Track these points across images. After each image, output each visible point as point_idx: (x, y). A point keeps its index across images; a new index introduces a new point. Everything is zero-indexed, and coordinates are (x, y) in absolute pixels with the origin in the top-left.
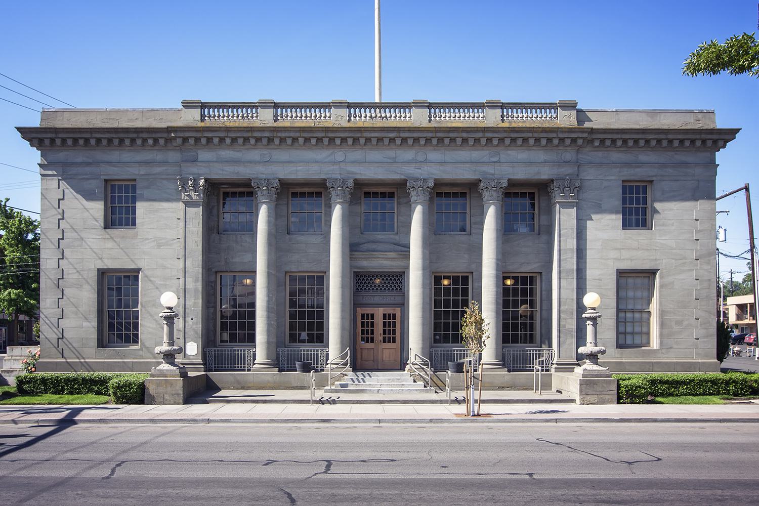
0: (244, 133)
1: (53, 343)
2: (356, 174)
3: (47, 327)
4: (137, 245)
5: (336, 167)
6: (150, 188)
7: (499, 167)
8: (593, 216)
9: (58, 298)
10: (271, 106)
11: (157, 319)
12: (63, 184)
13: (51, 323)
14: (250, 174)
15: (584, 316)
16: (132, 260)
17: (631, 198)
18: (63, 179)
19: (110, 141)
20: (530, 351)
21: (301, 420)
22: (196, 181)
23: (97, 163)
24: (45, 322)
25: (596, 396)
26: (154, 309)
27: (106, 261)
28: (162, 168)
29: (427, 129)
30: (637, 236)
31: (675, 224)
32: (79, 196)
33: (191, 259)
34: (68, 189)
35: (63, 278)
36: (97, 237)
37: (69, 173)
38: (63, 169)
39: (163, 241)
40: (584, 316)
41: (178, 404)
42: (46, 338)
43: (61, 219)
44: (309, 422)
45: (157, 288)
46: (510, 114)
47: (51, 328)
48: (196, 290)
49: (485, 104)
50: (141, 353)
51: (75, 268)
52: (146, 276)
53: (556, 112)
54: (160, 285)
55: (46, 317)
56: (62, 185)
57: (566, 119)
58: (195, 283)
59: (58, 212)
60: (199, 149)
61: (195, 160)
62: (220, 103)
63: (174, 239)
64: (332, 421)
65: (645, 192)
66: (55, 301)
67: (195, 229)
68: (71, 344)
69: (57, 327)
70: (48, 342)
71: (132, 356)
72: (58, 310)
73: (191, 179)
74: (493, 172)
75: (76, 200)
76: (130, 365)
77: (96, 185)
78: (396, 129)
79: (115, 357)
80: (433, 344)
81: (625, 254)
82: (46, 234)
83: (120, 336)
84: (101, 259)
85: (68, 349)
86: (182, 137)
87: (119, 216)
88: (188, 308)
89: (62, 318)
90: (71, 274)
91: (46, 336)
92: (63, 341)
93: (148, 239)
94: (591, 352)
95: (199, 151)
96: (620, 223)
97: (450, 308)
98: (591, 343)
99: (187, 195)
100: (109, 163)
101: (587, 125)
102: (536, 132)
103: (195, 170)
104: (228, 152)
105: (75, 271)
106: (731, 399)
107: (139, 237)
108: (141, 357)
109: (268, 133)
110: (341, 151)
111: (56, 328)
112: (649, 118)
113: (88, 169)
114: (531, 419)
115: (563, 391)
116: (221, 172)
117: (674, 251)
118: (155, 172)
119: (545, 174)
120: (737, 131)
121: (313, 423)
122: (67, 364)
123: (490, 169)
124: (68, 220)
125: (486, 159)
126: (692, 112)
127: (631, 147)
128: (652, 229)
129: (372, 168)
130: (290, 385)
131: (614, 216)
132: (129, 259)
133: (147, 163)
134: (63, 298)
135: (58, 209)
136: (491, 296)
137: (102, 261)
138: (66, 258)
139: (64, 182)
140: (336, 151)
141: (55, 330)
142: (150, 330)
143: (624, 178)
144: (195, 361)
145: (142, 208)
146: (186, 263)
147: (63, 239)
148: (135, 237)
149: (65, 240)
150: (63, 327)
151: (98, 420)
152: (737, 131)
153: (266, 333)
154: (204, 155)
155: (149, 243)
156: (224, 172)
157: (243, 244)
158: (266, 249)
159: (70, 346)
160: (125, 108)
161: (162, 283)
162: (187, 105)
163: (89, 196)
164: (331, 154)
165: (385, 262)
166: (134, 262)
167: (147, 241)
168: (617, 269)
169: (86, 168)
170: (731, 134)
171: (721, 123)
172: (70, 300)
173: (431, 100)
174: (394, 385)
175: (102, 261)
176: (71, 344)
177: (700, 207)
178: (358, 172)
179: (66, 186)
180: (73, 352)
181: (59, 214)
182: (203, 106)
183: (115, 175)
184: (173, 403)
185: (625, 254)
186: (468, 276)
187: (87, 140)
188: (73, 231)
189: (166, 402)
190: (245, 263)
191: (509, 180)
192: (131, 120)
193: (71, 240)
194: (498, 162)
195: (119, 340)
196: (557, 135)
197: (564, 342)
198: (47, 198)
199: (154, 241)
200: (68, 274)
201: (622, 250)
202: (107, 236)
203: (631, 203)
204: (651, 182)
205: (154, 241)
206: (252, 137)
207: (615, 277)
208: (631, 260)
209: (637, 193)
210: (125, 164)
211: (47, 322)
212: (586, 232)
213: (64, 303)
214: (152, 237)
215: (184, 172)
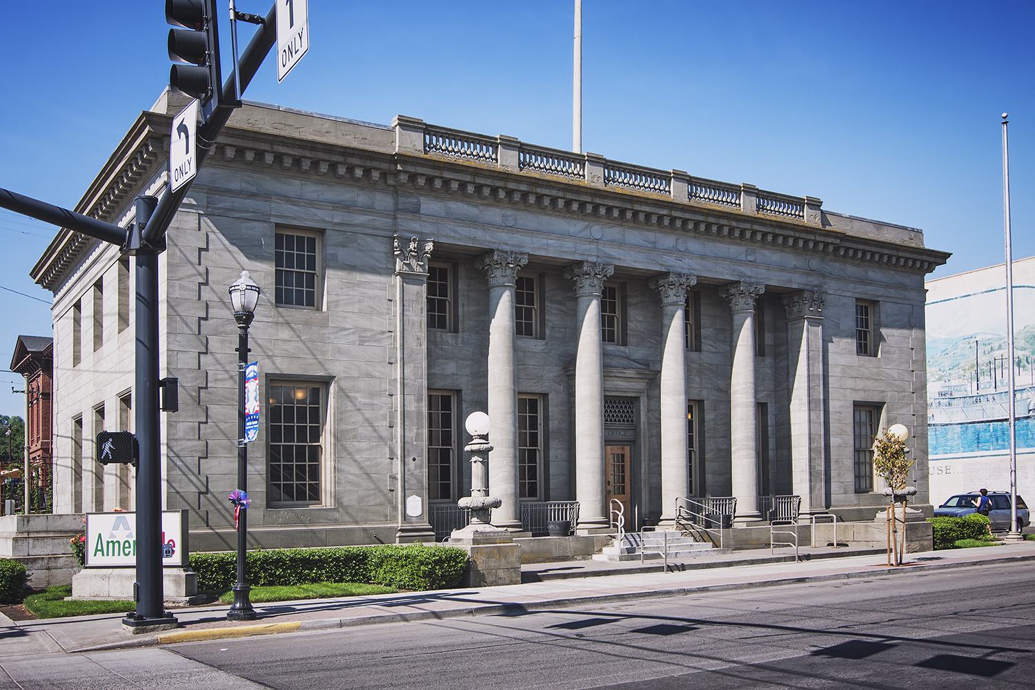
0: (496, 181)
3: (180, 473)
4: (329, 338)
6: (347, 247)
7: (755, 269)
10: (516, 147)
11: (359, 460)
12: (206, 223)
13: (186, 466)
14: (489, 242)
15: (467, 448)
16: (320, 363)
18: (206, 215)
20: (566, 506)
21: (778, 581)
23: (267, 196)
24: (176, 464)
25: (918, 542)
27: (278, 361)
28: (368, 217)
29: (701, 210)
30: (865, 359)
31: (896, 352)
32: (234, 249)
33: (413, 364)
34: (213, 232)
36: (265, 319)
38: (208, 198)
39: (368, 334)
40: (467, 448)
43: (203, 284)
44: (786, 584)
46: (434, 143)
47: (185, 475)
48: (419, 413)
49: (672, 175)
50: (337, 515)
52: (341, 389)
55: (178, 456)
56: (204, 224)
57: (809, 218)
58: (418, 403)
59: (198, 272)
60: (423, 195)
61: (416, 211)
62: (450, 130)
63: (384, 332)
64: (807, 580)
65: (312, 248)
68: (221, 504)
69: (197, 472)
70: (181, 500)
71: (321, 521)
72: (196, 443)
73: (414, 240)
74: (750, 274)
77: (263, 232)
78: (670, 205)
82: (177, 308)
83: (288, 490)
85: (216, 511)
86: (490, 186)
87: (296, 288)
88: (408, 442)
89: (206, 458)
91: (177, 489)
94: (483, 503)
95: (421, 198)
97: (281, 442)
98: (479, 491)
101: (828, 228)
103: (416, 226)
104: (461, 205)
105: (227, 376)
108: (336, 521)
109: (526, 186)
110: (598, 224)
111: (194, 475)
112: (875, 230)
113: (250, 203)
114: (962, 563)
115: (848, 543)
116: (453, 235)
117: (896, 382)
118: (355, 222)
119: (796, 282)
121: (790, 583)
122: (217, 537)
123: (747, 271)
124: (214, 287)
125: (743, 257)
126: (905, 228)
129: (632, 253)
130: (550, 555)
131: (850, 340)
132: (315, 360)
133: (347, 207)
134: (206, 423)
135: (197, 266)
136: (750, 430)
138: (211, 353)
140: (592, 224)
141: (193, 478)
145: (333, 282)
146: (405, 371)
147: (206, 319)
148: (324, 324)
149: (210, 322)
150: (207, 472)
151: (554, 601)
152: (949, 255)
154: (429, 205)
155: (346, 335)
156: (457, 235)
157: (443, 347)
159: (220, 507)
160: (839, 213)
161: (367, 401)
162: (407, 124)
164: (586, 227)
165: (620, 383)
166: (323, 366)
167: (344, 333)
168: (854, 401)
170: (942, 257)
171: (929, 243)
172: (217, 426)
173: (609, 156)
174: (683, 546)
176: (221, 504)
177: (915, 333)
178: (618, 256)
179: (210, 227)
180: (224, 516)
181: (200, 274)
182: (428, 130)
183: (294, 219)
184: (509, 582)
185: (860, 384)
186: (537, 400)
187: (260, 154)
188: (223, 306)
190: (448, 375)
193: (220, 321)
196: (752, 227)
197: (815, 487)
198: (179, 244)
199: (353, 333)
200: (216, 380)
201: (857, 379)
202: (281, 320)
203: (290, 265)
204: (322, 232)
206: (502, 188)
208: (865, 391)
209: (301, 248)
210: (309, 202)
211: (179, 463)
212: (828, 355)
213: (208, 431)
214: (352, 327)
215: (402, 228)
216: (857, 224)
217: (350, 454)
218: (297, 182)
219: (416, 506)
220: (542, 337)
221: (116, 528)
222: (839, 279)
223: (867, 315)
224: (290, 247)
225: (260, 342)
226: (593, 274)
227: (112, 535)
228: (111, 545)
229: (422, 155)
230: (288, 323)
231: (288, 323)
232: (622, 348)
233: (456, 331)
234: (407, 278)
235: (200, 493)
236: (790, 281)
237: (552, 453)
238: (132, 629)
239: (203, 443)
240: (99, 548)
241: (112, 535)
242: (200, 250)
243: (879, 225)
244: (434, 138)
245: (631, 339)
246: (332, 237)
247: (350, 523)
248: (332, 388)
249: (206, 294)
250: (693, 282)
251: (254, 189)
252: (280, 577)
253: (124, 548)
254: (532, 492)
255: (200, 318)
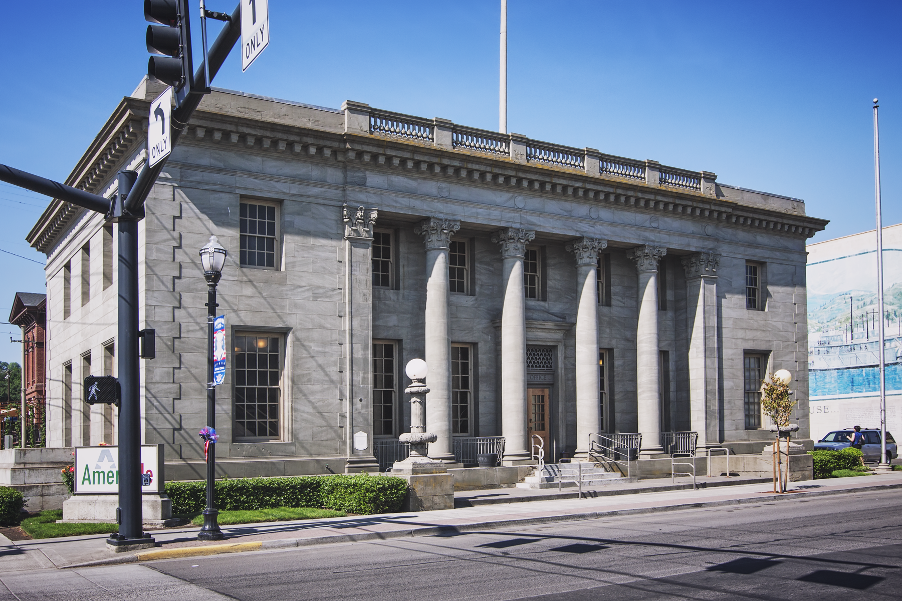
1: (166, 437)
2: (536, 225)
5: (517, 215)
8: (727, 296)
9: (174, 368)
10: (449, 128)
14: (427, 211)
16: (279, 316)
17: (253, 223)
18: (180, 187)
19: (259, 140)
22: (367, 212)
23: (233, 171)
26: (310, 387)
27: (242, 314)
32: (204, 217)
35: (180, 338)
37: (191, 179)
39: (321, 291)
40: (407, 390)
41: (450, 508)
42: (155, 429)
45: (313, 357)
48: (365, 360)
50: (293, 449)
51: (197, 323)
53: (432, 132)
54: (318, 352)
55: (155, 397)
57: (705, 190)
60: (369, 170)
66: (168, 373)
67: (363, 278)
68: (193, 439)
69: (171, 411)
72: (171, 385)
75: (198, 221)
76: (282, 467)
77: (229, 203)
79: (257, 456)
80: (393, 436)
81: (750, 335)
84: (234, 311)
89: (180, 399)
90: (193, 331)
92: (181, 435)
93: (301, 287)
96: (744, 302)
99: (354, 230)
100: (250, 173)
101: (721, 198)
102: (695, 201)
103: (362, 197)
105: (197, 328)
106: (369, 522)
107: (288, 283)
108: (293, 454)
113: (218, 177)
118: (309, 193)
119: (694, 245)
120: (826, 222)
122: (189, 468)
123: (651, 236)
124: (187, 250)
126: (789, 199)
127: (251, 147)
128: (763, 310)
131: (740, 297)
133: (303, 180)
134: (180, 368)
137: (238, 315)
138: (184, 308)
139: (181, 192)
141: (168, 416)
142: (305, 415)
143: (747, 258)
144: (365, 458)
147: (180, 278)
149: (183, 280)
150: (180, 412)
152: (826, 222)
153: (447, 419)
154: (374, 179)
158: (446, 310)
159: (191, 441)
161: (320, 349)
162: (355, 108)
163: (220, 219)
165: (540, 334)
167: (300, 290)
169: (215, 175)
170: (820, 224)
173: (456, 121)
175: (238, 315)
176: (193, 439)
177: (797, 290)
178: (538, 223)
181: (174, 239)
182: (373, 113)
183: (256, 190)
185: (750, 335)
187: (226, 135)
189: (436, 507)
191: (668, 249)
192: (277, 115)
194: (657, 228)
195: (250, 433)
199: (308, 290)
200: (188, 331)
202: (245, 278)
204: (280, 202)
205: (308, 290)
207: (742, 357)
208: (754, 340)
209: (262, 216)
210: (270, 176)
211: (156, 403)
213: (182, 375)
216: (747, 196)
217: (305, 395)
218: (259, 159)
219: (362, 441)
220: (473, 294)
221: (101, 459)
222: (731, 242)
223: (755, 274)
224: (253, 215)
225: (227, 298)
226: (516, 238)
227: (98, 466)
228: (96, 474)
229: (368, 135)
230: (251, 281)
231: (251, 281)
232: (542, 303)
233: (397, 288)
234: (355, 242)
235: (174, 429)
236: (688, 245)
237: (481, 395)
238: (115, 548)
239: (176, 386)
240: (87, 477)
241: (98, 466)
242: (175, 218)
243: (766, 196)
244: (378, 120)
245: (550, 296)
246: (289, 206)
247: (305, 456)
248: (290, 338)
249: (180, 256)
250: (604, 246)
251: (221, 165)
252: (244, 502)
253: (108, 477)
254: (464, 429)
255: (174, 278)
